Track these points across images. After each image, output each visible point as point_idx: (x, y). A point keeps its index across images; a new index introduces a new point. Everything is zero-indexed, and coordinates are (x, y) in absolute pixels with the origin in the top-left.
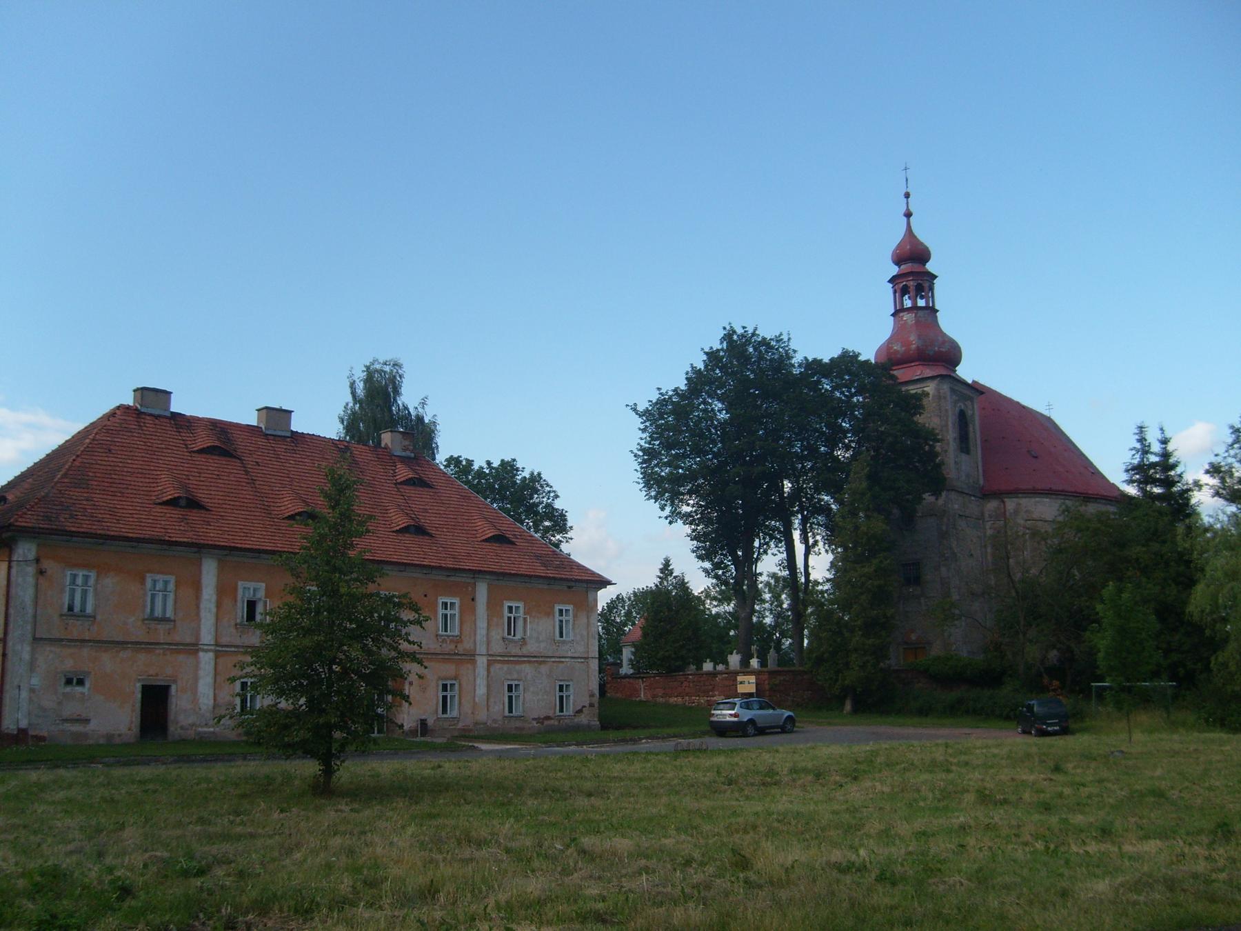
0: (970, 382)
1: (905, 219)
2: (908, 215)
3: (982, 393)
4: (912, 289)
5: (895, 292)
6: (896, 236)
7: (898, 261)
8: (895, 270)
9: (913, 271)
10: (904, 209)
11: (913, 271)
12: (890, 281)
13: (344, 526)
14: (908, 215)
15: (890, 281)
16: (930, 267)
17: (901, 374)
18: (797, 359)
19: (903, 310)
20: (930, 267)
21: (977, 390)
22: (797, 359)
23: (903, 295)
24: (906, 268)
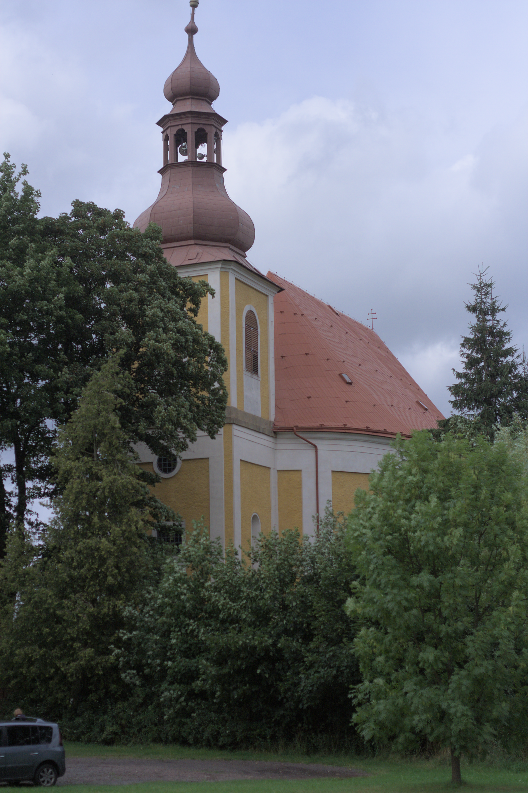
0: (265, 273)
1: (186, 36)
2: (192, 30)
3: (281, 290)
4: (190, 137)
5: (166, 139)
6: (172, 59)
7: (174, 95)
8: (167, 108)
9: (193, 117)
10: (187, 22)
11: (193, 117)
12: (159, 123)
13: (15, 333)
14: (192, 30)
15: (159, 123)
16: (218, 107)
17: (174, 257)
18: (201, 299)
19: (176, 165)
20: (218, 107)
21: (273, 284)
22: (201, 299)
23: (177, 143)
24: (187, 106)
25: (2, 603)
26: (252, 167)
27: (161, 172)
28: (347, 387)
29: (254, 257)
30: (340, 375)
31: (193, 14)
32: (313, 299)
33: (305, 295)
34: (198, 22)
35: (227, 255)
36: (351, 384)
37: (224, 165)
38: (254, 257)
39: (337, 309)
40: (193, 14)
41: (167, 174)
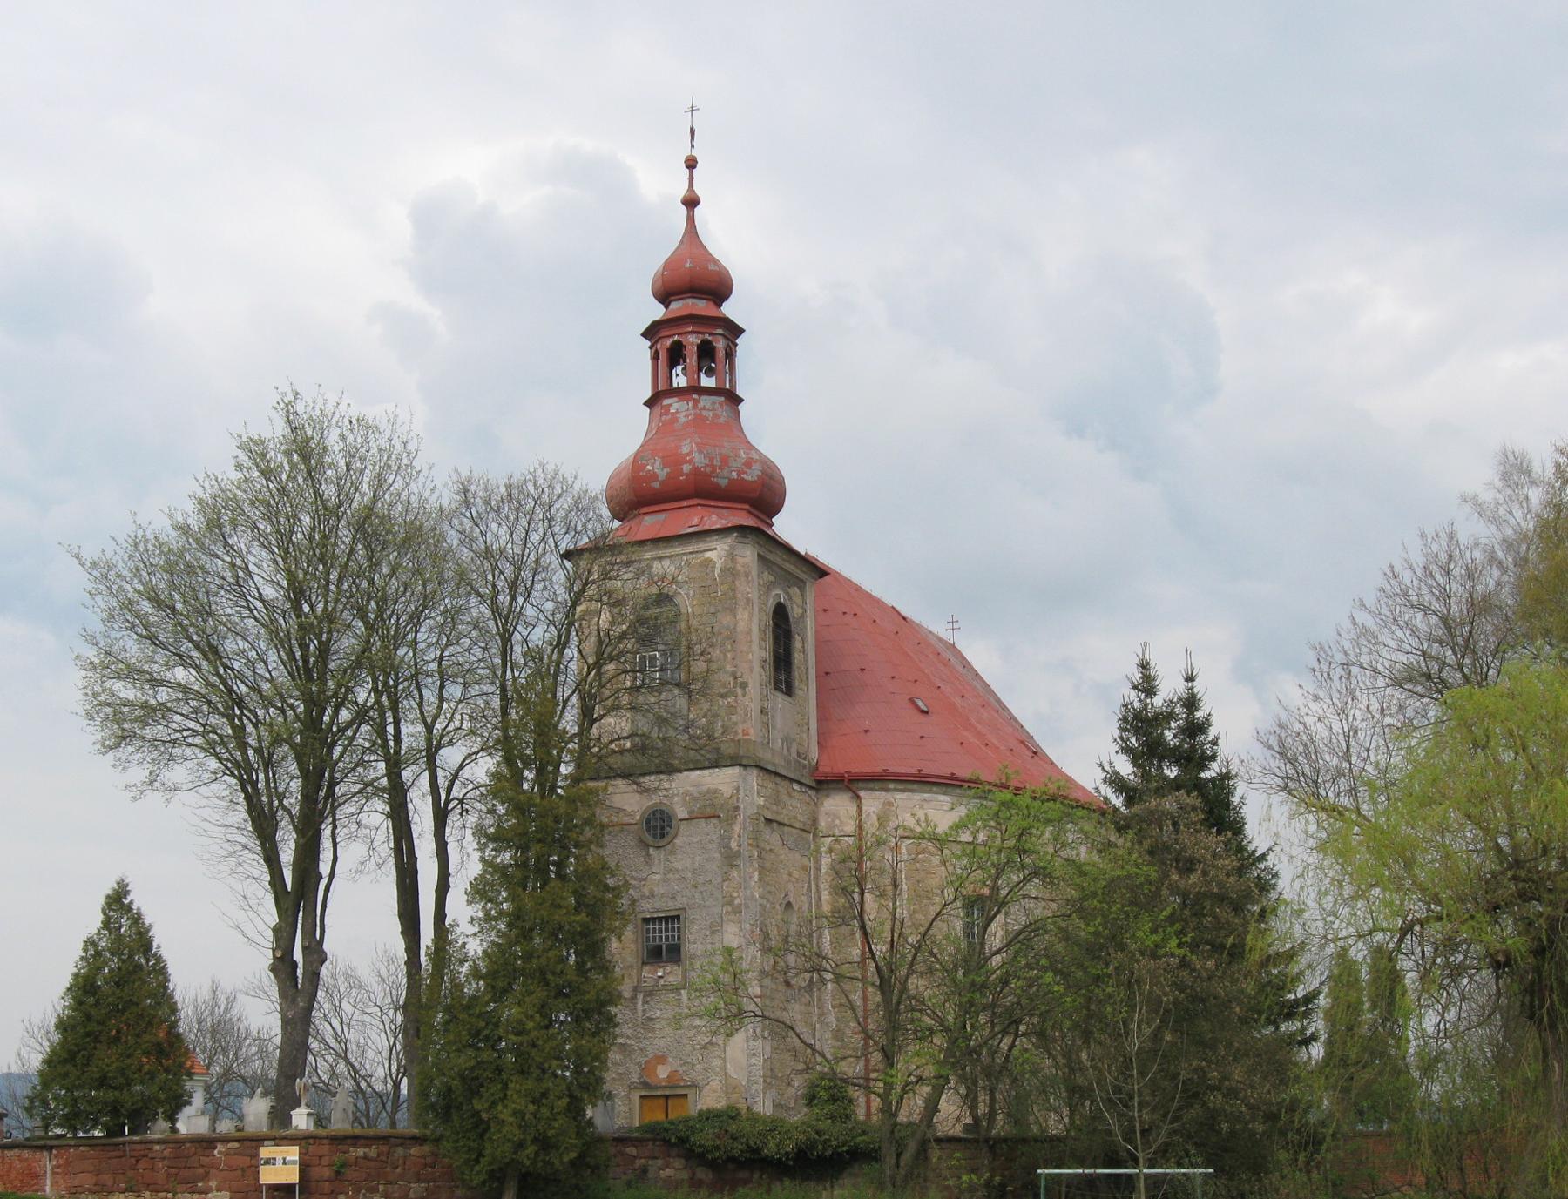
5: (656, 357)
8: (658, 312)
10: (682, 191)
12: (645, 335)
14: (691, 164)
15: (645, 335)
25: (1235, 1153)
26: (781, 410)
27: (650, 403)
28: (923, 718)
29: (785, 526)
30: (912, 701)
31: (691, 220)
32: (869, 595)
33: (858, 589)
34: (699, 190)
35: (749, 521)
36: (926, 712)
37: (739, 392)
38: (785, 526)
39: (903, 613)
40: (691, 220)
41: (658, 409)
